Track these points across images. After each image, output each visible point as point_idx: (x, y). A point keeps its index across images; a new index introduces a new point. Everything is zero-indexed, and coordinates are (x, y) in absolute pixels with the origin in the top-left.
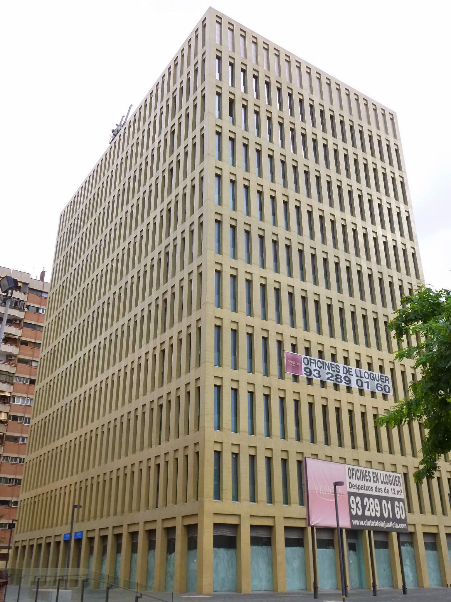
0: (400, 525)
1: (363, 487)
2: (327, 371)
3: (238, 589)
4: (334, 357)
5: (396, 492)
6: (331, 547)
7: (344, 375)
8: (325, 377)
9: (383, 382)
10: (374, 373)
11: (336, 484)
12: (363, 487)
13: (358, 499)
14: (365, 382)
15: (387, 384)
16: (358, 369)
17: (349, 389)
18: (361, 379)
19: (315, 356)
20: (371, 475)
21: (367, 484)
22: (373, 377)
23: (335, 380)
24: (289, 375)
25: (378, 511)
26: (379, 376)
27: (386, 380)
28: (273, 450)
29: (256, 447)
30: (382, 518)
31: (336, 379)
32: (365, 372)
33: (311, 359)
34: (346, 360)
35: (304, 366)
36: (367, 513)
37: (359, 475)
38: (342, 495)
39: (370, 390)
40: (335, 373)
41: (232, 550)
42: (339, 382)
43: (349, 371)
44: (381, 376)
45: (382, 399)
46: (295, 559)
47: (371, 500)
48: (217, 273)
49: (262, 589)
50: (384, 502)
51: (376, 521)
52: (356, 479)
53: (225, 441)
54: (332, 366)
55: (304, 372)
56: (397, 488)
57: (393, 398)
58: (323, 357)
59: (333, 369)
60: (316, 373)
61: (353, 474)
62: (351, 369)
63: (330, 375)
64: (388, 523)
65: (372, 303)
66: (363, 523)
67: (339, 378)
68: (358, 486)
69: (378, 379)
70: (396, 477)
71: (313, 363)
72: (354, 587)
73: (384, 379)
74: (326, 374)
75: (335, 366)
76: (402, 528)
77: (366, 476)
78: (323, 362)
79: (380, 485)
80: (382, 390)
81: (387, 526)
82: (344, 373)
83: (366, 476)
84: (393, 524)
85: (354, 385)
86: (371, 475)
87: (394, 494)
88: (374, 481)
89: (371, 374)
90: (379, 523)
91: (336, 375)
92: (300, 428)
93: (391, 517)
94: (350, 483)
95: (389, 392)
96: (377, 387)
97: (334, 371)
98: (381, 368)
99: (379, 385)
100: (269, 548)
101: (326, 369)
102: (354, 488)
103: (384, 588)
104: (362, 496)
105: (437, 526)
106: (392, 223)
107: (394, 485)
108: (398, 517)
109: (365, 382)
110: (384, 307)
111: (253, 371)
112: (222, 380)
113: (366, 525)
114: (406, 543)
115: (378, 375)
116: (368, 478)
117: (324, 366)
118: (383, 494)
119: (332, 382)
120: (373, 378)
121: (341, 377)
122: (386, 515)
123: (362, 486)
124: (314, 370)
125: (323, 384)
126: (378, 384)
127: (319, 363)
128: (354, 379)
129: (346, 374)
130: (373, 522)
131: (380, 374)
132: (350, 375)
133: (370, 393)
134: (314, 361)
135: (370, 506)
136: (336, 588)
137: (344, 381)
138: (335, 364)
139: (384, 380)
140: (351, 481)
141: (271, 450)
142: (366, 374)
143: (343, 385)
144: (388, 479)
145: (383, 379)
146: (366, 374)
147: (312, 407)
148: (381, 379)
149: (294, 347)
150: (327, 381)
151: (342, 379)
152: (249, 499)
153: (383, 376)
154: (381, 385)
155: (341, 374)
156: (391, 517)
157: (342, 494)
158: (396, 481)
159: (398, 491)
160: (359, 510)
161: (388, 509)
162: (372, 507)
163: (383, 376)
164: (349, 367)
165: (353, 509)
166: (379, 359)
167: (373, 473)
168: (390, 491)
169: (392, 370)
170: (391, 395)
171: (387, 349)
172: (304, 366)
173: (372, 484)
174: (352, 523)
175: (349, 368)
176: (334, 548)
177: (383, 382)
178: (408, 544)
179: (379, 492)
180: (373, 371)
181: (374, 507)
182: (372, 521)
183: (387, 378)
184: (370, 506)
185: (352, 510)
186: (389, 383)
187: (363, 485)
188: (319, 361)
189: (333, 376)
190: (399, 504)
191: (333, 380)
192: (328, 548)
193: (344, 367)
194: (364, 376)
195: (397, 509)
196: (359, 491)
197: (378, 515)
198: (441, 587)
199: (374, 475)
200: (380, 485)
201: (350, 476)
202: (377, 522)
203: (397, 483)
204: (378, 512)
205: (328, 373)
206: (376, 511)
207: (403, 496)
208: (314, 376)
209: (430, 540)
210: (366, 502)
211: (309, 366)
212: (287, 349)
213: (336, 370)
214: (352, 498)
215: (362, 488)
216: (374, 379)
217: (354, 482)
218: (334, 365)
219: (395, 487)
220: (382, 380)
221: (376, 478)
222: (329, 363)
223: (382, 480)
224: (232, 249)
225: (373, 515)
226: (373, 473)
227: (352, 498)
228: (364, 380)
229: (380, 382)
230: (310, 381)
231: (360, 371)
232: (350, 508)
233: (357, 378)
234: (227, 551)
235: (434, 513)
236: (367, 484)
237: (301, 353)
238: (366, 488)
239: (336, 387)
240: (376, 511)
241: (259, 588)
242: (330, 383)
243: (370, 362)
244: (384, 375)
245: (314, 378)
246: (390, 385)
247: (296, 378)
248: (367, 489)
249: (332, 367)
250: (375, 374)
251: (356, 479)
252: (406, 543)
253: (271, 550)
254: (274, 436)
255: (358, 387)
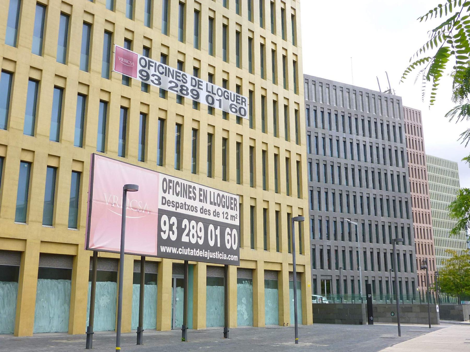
0: (229, 256)
1: (183, 206)
2: (170, 79)
3: (14, 332)
4: (181, 64)
5: (229, 217)
6: (153, 283)
7: (192, 88)
8: (166, 85)
9: (239, 103)
10: (229, 92)
11: (127, 189)
12: (183, 206)
13: (174, 219)
14: (217, 100)
15: (243, 106)
16: (210, 84)
17: (196, 105)
18: (213, 95)
19: (156, 58)
20: (197, 192)
21: (190, 202)
22: (227, 96)
23: (179, 92)
24: (117, 75)
25: (200, 238)
26: (234, 96)
27: (242, 101)
28: (85, 163)
29: (59, 157)
30: (206, 246)
31: (181, 90)
32: (219, 89)
33: (149, 61)
34: (196, 71)
35: (139, 68)
36: (185, 239)
37: (178, 189)
38: (148, 213)
39: (222, 109)
40: (180, 84)
41: (11, 283)
42: (184, 94)
43: (198, 84)
44: (237, 96)
45: (235, 121)
46: (103, 295)
47: (193, 223)
48: (127, 43)
49: (52, 331)
50: (211, 227)
51: (196, 250)
52: (173, 194)
53: (11, 144)
54: (178, 74)
55: (138, 75)
56: (231, 212)
57: (248, 122)
58: (167, 62)
59: (178, 78)
60: (156, 79)
61: (170, 187)
62: (202, 82)
63: (173, 85)
64: (214, 253)
65: (236, 13)
66: (178, 250)
67: (184, 90)
68: (175, 204)
69: (233, 99)
70: (232, 198)
71: (152, 66)
72: (178, 326)
73: (241, 100)
74: (167, 83)
75: (181, 75)
76: (232, 260)
77: (190, 192)
78: (166, 67)
79: (207, 206)
80: (236, 112)
81: (211, 257)
82: (192, 85)
83: (190, 192)
84: (221, 254)
85: (202, 100)
86: (197, 192)
87: (227, 218)
88: (200, 200)
89: (225, 91)
90: (201, 251)
91: (182, 86)
92: (126, 143)
93: (219, 245)
94: (163, 198)
95: (245, 115)
96: (231, 108)
97: (180, 81)
98: (239, 88)
99: (233, 106)
100: (67, 282)
101: (169, 76)
102: (169, 206)
103: (213, 328)
104: (180, 217)
105: (281, 263)
106: (295, 42)
107: (228, 208)
108: (228, 246)
109: (217, 100)
110: (275, 84)
111: (66, 62)
112: (16, 65)
113: (180, 253)
114: (245, 280)
115: (234, 95)
116: (192, 195)
117: (167, 72)
118: (211, 217)
119: (176, 93)
120: (227, 97)
121: (187, 89)
122: (212, 243)
123: (181, 204)
124: (153, 75)
125: (164, 93)
126: (232, 105)
127: (161, 68)
128: (203, 94)
129: (195, 86)
130: (192, 250)
131: (236, 94)
132: (199, 88)
133: (222, 113)
134: (154, 65)
135: (190, 231)
136: (154, 328)
137: (190, 94)
138: (182, 73)
139: (240, 102)
140: (166, 195)
141: (82, 163)
142: (220, 91)
143: (189, 99)
144: (221, 201)
145: (239, 100)
146: (220, 91)
147: (146, 119)
148: (237, 99)
149: (129, 42)
150: (169, 90)
151: (189, 91)
152: (41, 220)
153: (240, 97)
154: (237, 107)
155: (188, 85)
156: (219, 245)
157: (145, 211)
158: (232, 203)
159: (231, 216)
160: (173, 234)
161: (216, 236)
162: (193, 231)
163: (240, 97)
164: (199, 79)
165: (165, 232)
166: (237, 77)
167: (200, 190)
168: (221, 215)
169: (251, 92)
170: (246, 119)
171: (248, 68)
172: (139, 68)
173: (196, 203)
174: (159, 249)
175: (199, 81)
176: (156, 284)
177: (239, 103)
178: (246, 281)
179: (206, 214)
180: (229, 89)
181: (197, 232)
182: (190, 249)
183: (244, 100)
184: (190, 231)
185: (162, 233)
186: (245, 106)
187: (184, 203)
188: (160, 65)
189: (177, 86)
190: (231, 232)
191: (177, 91)
192: (149, 284)
193: (192, 78)
194: (216, 93)
195: (227, 237)
196: (176, 210)
197: (201, 242)
198: (276, 326)
199: (202, 193)
200: (207, 206)
201: (165, 189)
202: (198, 251)
203: (233, 206)
204: (201, 239)
205: (171, 82)
206: (198, 237)
207: (237, 223)
208: (152, 81)
209: (271, 278)
210: (185, 225)
211: (146, 69)
212: (119, 43)
213: (182, 80)
214: (165, 218)
215: (181, 206)
216: (228, 99)
217: (170, 197)
218: (180, 73)
219: (229, 211)
220: (238, 101)
221: (204, 197)
222: (173, 71)
223: (212, 200)
224: (129, 6)
225: (193, 241)
226: (200, 190)
227: (165, 218)
228: (216, 97)
229: (235, 103)
230: (146, 87)
231: (212, 86)
232: (160, 230)
233: (208, 94)
234: (3, 284)
235: (280, 250)
236: (190, 202)
237: (138, 52)
238: (187, 207)
239: (180, 99)
240: (198, 237)
241: (48, 330)
242: (172, 94)
243: (265, 149)
244: (241, 96)
245: (151, 84)
246: (247, 108)
247: (127, 80)
248: (188, 209)
249: (177, 76)
250: (231, 93)
251: (173, 194)
252: (245, 280)
253: (69, 285)
254: (88, 146)
255: (207, 104)
